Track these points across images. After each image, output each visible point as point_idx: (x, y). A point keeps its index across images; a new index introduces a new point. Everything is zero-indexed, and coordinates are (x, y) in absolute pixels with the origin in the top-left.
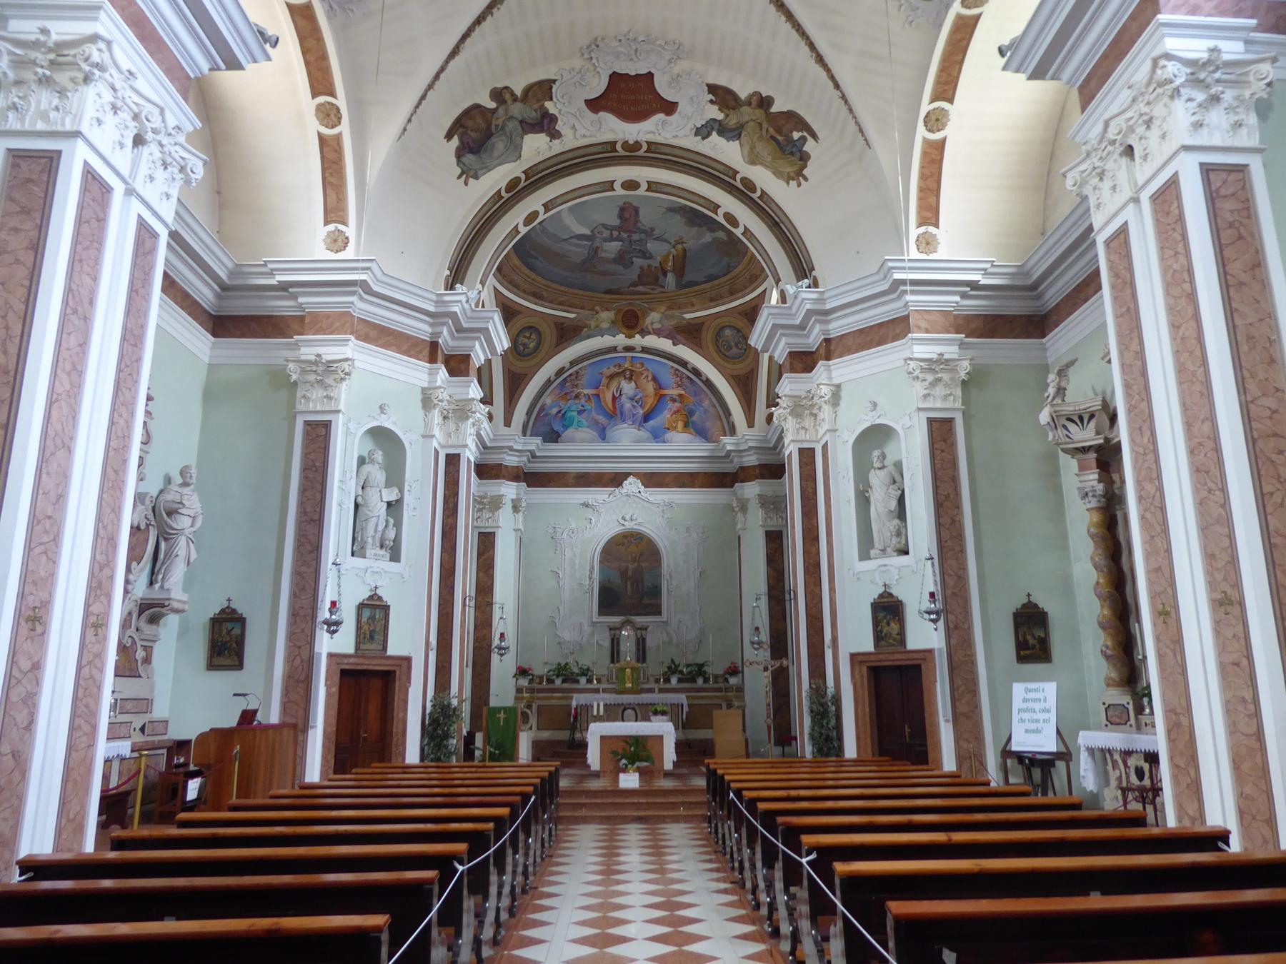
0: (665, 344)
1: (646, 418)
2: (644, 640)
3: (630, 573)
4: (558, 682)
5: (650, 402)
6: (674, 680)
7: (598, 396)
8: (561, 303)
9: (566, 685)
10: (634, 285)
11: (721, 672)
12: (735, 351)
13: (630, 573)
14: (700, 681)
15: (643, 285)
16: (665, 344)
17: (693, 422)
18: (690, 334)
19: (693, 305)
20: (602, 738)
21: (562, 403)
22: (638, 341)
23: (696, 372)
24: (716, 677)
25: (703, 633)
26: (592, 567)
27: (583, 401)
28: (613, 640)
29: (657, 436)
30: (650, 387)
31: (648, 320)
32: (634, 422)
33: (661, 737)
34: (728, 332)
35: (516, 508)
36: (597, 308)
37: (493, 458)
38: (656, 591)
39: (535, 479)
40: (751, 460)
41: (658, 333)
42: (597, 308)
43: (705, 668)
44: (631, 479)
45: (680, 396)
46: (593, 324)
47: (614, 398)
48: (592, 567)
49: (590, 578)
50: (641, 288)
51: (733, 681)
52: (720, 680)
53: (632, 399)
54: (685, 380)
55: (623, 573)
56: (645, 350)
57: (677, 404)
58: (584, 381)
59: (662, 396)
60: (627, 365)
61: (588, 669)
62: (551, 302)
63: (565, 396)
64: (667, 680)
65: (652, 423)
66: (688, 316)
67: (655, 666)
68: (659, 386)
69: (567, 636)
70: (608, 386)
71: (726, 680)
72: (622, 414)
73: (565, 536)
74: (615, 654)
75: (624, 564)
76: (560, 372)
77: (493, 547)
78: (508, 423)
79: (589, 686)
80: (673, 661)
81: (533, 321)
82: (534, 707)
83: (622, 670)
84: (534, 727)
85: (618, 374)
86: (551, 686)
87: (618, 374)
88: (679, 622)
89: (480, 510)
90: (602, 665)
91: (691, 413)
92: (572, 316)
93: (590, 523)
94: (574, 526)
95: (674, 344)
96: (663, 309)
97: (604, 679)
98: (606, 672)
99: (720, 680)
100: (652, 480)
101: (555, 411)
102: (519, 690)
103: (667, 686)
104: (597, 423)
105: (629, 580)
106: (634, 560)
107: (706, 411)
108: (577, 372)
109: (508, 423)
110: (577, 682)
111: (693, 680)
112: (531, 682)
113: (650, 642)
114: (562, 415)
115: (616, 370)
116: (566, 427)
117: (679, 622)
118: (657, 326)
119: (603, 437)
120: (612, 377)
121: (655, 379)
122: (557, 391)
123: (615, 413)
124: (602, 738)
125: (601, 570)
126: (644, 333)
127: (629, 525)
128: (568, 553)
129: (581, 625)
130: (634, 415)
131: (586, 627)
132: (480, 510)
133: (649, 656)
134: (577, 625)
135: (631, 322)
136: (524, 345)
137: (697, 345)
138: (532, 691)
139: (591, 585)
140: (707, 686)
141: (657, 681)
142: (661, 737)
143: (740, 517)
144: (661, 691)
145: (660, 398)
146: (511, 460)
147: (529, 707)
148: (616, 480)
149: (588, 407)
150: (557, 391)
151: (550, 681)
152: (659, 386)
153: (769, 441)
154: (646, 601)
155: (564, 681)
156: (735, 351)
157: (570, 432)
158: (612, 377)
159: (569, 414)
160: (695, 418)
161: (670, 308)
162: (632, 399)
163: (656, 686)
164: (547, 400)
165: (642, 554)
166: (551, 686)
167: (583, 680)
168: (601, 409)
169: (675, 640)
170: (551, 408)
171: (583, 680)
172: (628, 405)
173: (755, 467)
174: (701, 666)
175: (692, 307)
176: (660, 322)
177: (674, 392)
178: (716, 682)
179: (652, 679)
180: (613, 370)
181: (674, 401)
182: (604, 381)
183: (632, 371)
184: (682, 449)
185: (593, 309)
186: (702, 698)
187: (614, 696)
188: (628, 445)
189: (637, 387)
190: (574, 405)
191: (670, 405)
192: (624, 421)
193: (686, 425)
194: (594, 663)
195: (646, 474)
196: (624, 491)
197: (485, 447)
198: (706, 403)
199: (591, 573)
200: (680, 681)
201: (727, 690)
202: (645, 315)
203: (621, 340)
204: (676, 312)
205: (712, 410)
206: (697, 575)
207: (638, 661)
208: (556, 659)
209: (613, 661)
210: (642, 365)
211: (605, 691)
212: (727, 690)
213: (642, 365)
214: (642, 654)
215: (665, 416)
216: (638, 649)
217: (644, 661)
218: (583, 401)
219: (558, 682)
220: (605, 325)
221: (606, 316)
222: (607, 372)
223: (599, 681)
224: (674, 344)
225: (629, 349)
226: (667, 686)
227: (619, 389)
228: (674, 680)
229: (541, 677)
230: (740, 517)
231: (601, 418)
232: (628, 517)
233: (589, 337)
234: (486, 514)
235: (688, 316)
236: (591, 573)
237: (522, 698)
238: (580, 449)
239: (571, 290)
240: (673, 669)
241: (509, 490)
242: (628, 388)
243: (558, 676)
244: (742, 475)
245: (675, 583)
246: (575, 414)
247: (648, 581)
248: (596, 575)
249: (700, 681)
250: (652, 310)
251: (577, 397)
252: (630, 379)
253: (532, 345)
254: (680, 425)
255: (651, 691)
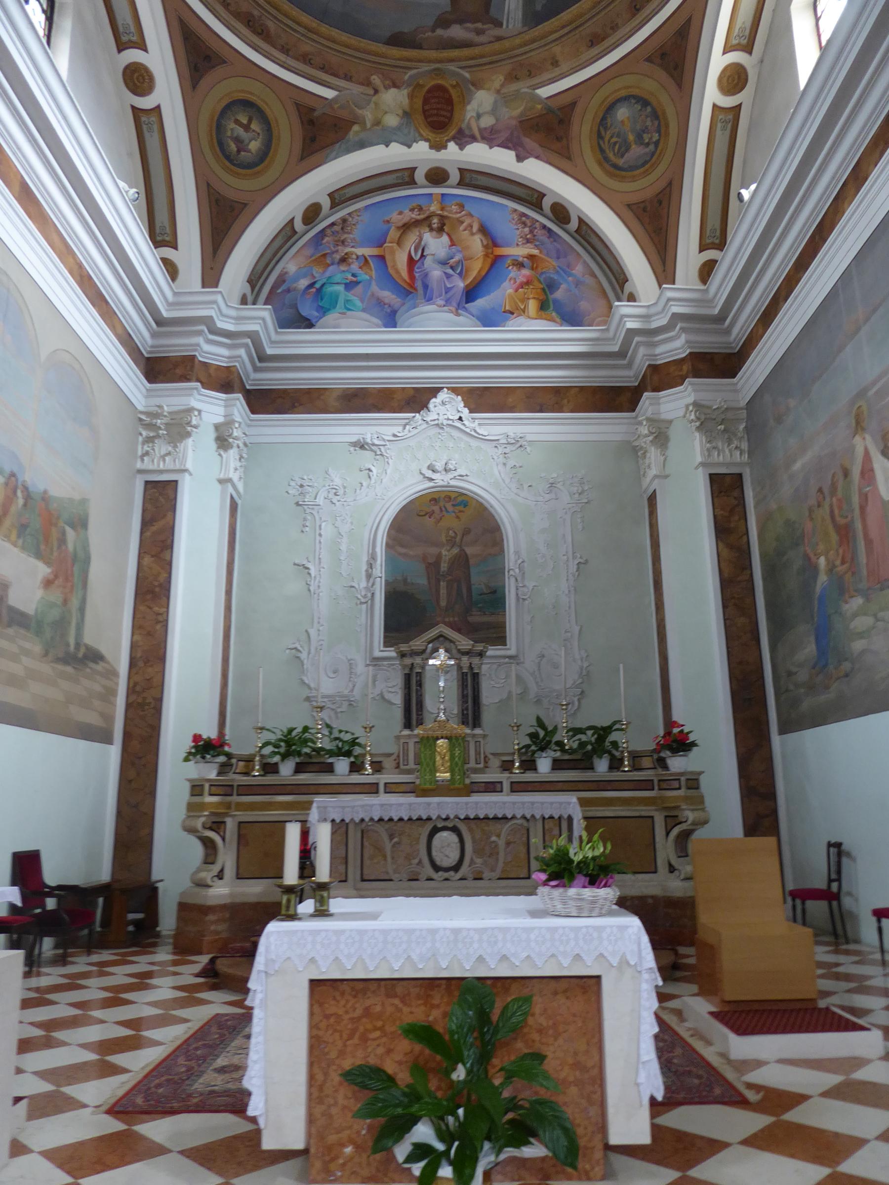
0: (500, 160)
1: (471, 294)
2: (476, 676)
3: (444, 567)
4: (287, 769)
5: (476, 267)
6: (544, 764)
7: (382, 258)
8: (305, 59)
9: (303, 778)
10: (443, 22)
11: (652, 746)
12: (636, 151)
13: (444, 567)
14: (602, 765)
15: (461, 21)
16: (500, 160)
17: (555, 301)
18: (547, 131)
19: (555, 63)
20: (320, 988)
21: (317, 271)
22: (453, 155)
23: (560, 213)
24: (635, 757)
25: (586, 676)
26: (373, 556)
27: (355, 267)
28: (408, 678)
29: (488, 320)
30: (476, 244)
31: (471, 110)
32: (448, 302)
33: (588, 987)
34: (622, 113)
35: (223, 441)
36: (376, 79)
37: (177, 345)
38: (495, 599)
39: (263, 401)
40: (674, 347)
41: (490, 137)
42: (376, 79)
43: (614, 736)
44: (443, 396)
45: (531, 257)
46: (368, 115)
47: (411, 262)
48: (373, 556)
49: (369, 576)
50: (457, 32)
51: (677, 764)
52: (647, 762)
53: (444, 263)
54: (539, 232)
55: (432, 567)
56: (471, 178)
57: (526, 272)
58: (357, 233)
59: (498, 259)
60: (434, 208)
61: (354, 743)
62: (285, 50)
63: (322, 260)
64: (529, 765)
65: (481, 303)
66: (545, 92)
67: (501, 733)
68: (492, 241)
69: (328, 686)
70: (399, 242)
71: (662, 763)
72: (426, 287)
73: (320, 500)
74: (413, 711)
75: (433, 551)
76: (312, 213)
77: (174, 509)
78: (211, 276)
79: (356, 778)
80: (540, 723)
81: (256, 91)
82: (230, 825)
83: (429, 742)
84: (229, 872)
85: (417, 223)
86: (270, 779)
87: (417, 223)
88: (546, 655)
89: (149, 440)
90: (382, 733)
91: (551, 286)
92: (329, 94)
93: (370, 478)
94: (338, 481)
95: (520, 159)
96: (498, 80)
97: (388, 763)
98: (392, 748)
99: (647, 762)
100: (481, 399)
101: (303, 283)
102: (196, 788)
103: (529, 776)
104: (380, 303)
105: (443, 583)
106: (452, 542)
107: (578, 284)
108: (344, 220)
109: (211, 276)
110: (329, 769)
111: (584, 762)
112: (224, 769)
113: (489, 695)
114: (317, 291)
115: (415, 216)
116: (323, 311)
117: (546, 655)
118: (487, 121)
119: (391, 319)
120: (406, 228)
121: (484, 230)
122: (309, 252)
123: (412, 287)
124: (320, 988)
125: (390, 560)
126: (463, 138)
127: (441, 479)
128: (327, 530)
129: (351, 664)
130: (448, 290)
131: (360, 668)
132: (149, 440)
133: (487, 716)
134: (335, 657)
135: (438, 115)
136: (238, 140)
137: (559, 151)
138: (227, 790)
139: (370, 589)
140: (616, 775)
141: (507, 766)
142: (588, 987)
143: (653, 454)
144: (517, 787)
145: (495, 262)
146: (213, 352)
147: (217, 825)
148: (416, 400)
149: (363, 276)
150: (309, 252)
151: (270, 769)
152: (492, 241)
153: (709, 303)
154: (476, 618)
155: (299, 769)
156: (636, 151)
157: (330, 317)
158: (406, 228)
159: (329, 289)
160: (559, 294)
161: (512, 77)
162: (444, 263)
163: (504, 778)
164: (290, 265)
165: (467, 532)
166: (270, 779)
167: (342, 765)
168: (389, 279)
169: (533, 689)
170: (296, 279)
171: (342, 765)
172: (436, 273)
173: (683, 360)
174: (603, 732)
175: (554, 66)
176: (494, 112)
177: (520, 251)
178: (635, 768)
179: (495, 763)
180: (409, 216)
181: (520, 265)
182: (393, 234)
183: (442, 218)
184: (535, 342)
185: (368, 83)
186: (610, 802)
187: (411, 799)
188: (437, 332)
189: (453, 244)
190: (339, 274)
191: (513, 272)
192: (429, 299)
193: (543, 306)
194: (369, 729)
195: (472, 391)
196: (431, 417)
197: (160, 322)
198: (578, 270)
199: (371, 566)
200: (557, 765)
201: (665, 784)
202: (465, 100)
203: (420, 153)
204: (522, 86)
205: (589, 280)
206: (573, 568)
207: (464, 722)
208: (296, 718)
209: (408, 725)
210: (462, 207)
211: (390, 788)
212: (665, 784)
213: (462, 207)
214: (471, 710)
215: (504, 291)
216: (464, 697)
217: (476, 722)
218: (355, 267)
219: (287, 769)
220: (392, 121)
221: (394, 99)
222: (397, 218)
223: (378, 767)
224: (520, 159)
225: (437, 176)
226: (529, 776)
227: (421, 248)
228: (544, 764)
229: (249, 760)
230: (653, 454)
231: (387, 295)
232: (439, 466)
233: (362, 145)
234: (161, 448)
235: (545, 92)
236: (371, 566)
237: (202, 806)
238: (348, 341)
239: (324, 29)
240: (541, 739)
241: (210, 408)
242: (436, 245)
243: (285, 756)
244: (661, 377)
245: (530, 584)
246: (341, 288)
247: (478, 581)
248: (379, 570)
249: (602, 765)
250: (478, 85)
251: (344, 260)
252: (440, 230)
253: (254, 146)
254: (532, 305)
255: (492, 787)
